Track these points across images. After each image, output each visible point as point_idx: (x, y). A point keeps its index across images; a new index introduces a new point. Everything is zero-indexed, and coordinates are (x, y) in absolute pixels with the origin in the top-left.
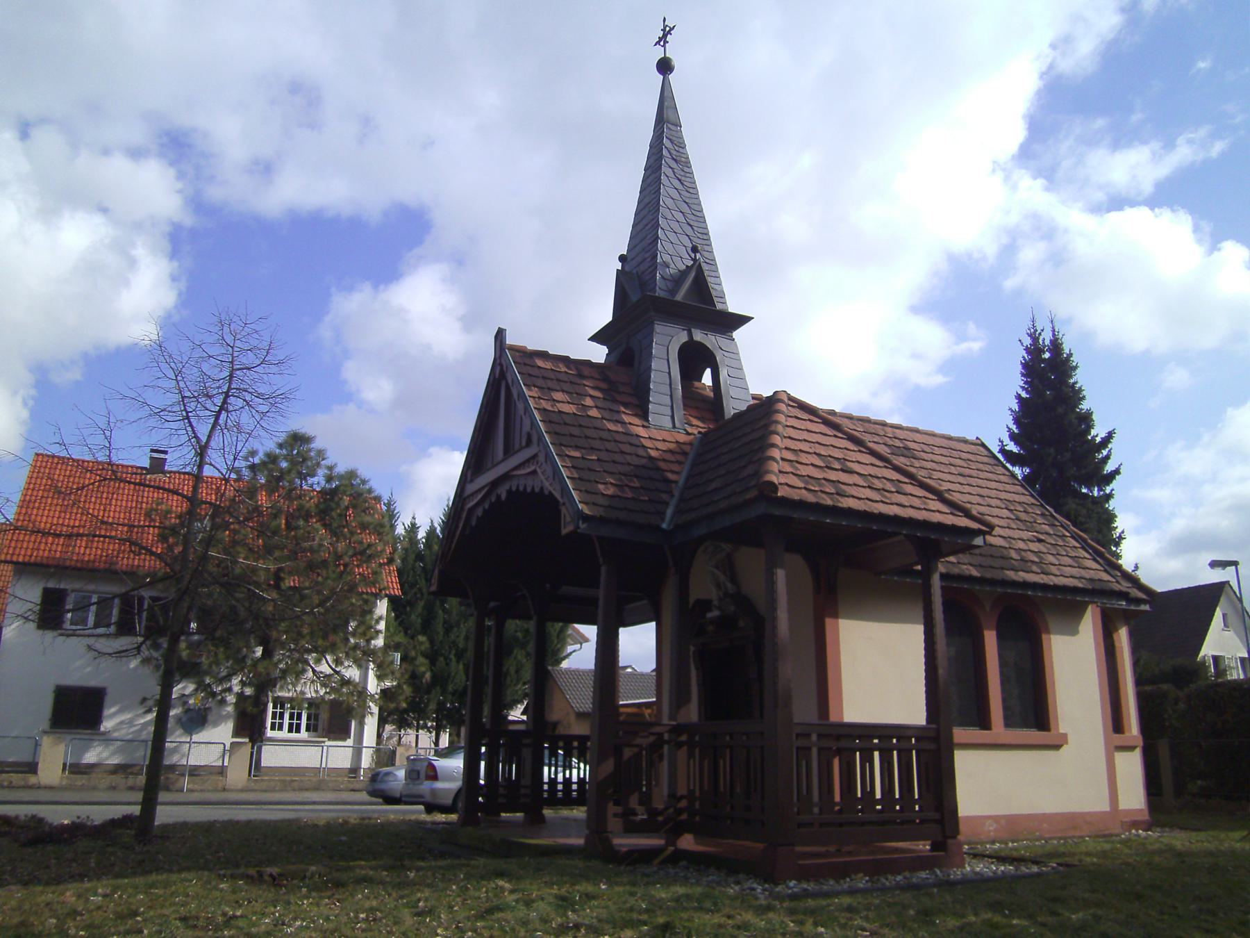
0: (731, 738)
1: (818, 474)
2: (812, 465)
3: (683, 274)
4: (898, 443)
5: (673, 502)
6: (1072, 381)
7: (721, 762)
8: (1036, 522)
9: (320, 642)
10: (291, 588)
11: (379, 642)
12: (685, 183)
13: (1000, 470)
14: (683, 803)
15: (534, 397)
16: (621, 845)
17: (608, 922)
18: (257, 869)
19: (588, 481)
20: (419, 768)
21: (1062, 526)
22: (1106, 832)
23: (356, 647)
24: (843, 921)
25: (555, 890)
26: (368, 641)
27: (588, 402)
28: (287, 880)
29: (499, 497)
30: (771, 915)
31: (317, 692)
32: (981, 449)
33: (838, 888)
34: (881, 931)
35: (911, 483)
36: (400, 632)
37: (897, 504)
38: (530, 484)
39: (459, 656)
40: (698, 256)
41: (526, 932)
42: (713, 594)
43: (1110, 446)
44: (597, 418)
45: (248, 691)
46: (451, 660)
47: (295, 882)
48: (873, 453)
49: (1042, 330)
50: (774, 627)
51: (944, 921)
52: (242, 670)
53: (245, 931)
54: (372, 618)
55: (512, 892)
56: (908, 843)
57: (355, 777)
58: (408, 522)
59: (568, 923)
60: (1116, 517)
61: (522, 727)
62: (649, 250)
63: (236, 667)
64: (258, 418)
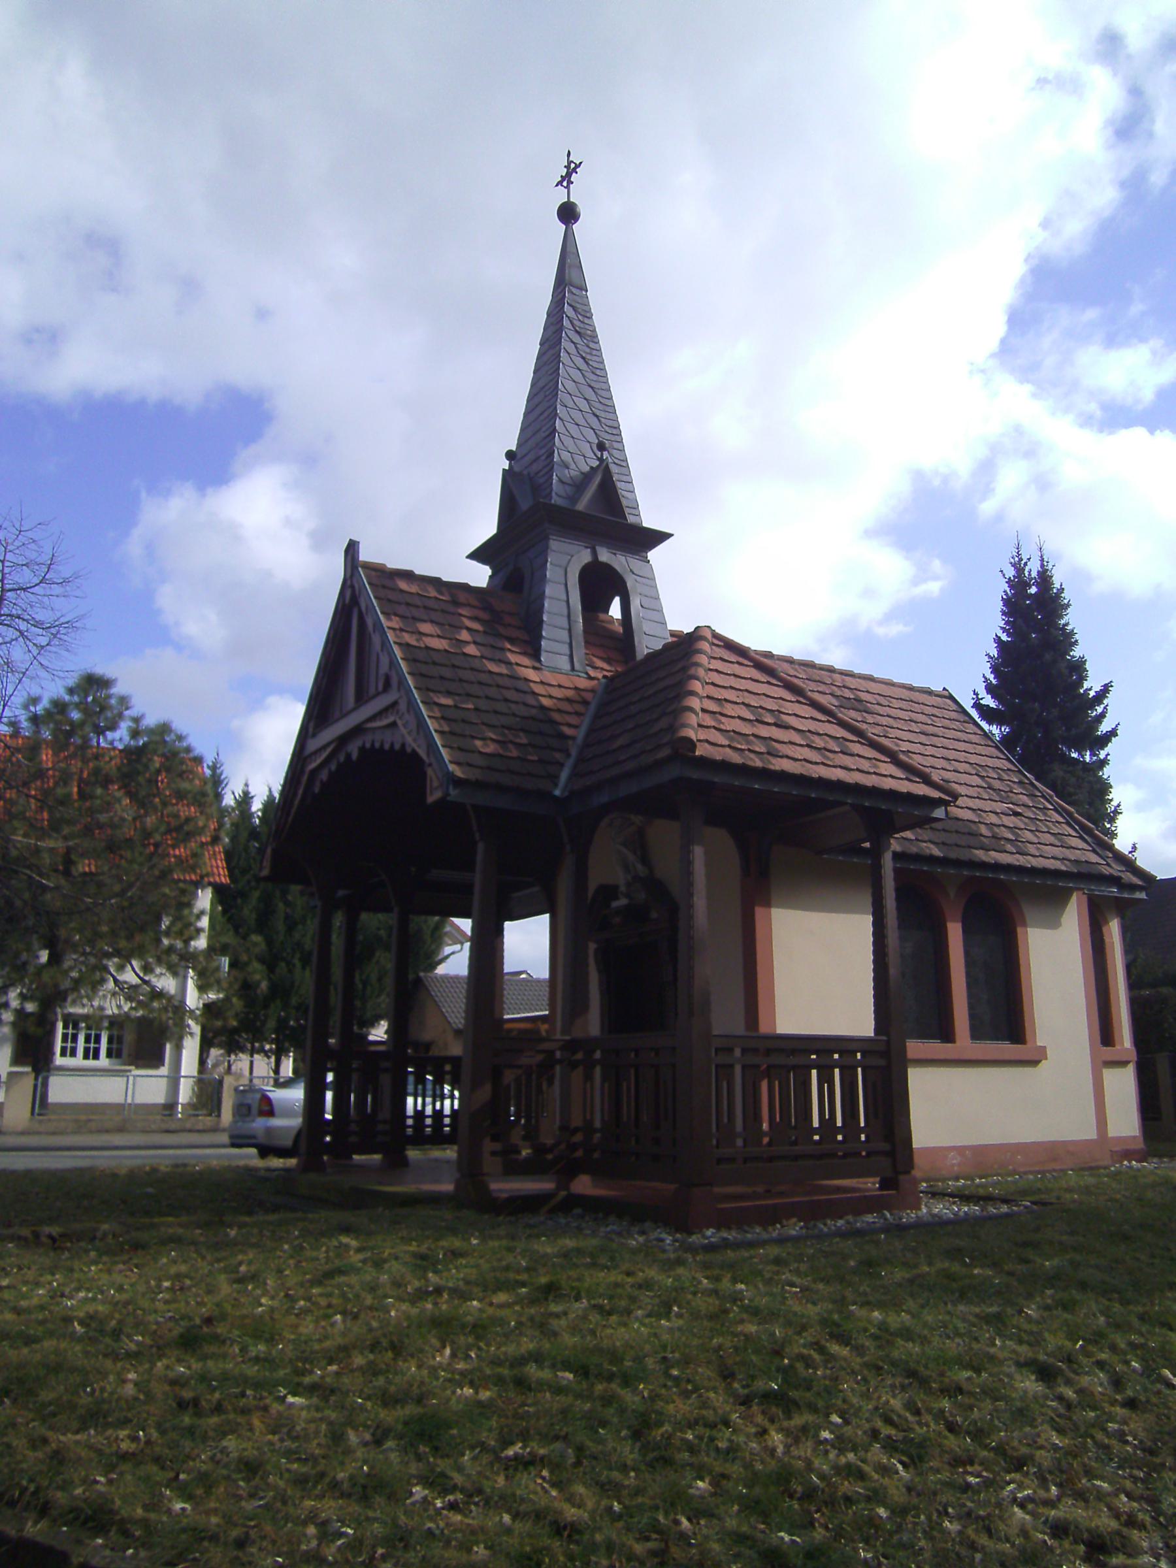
0: (636, 1055)
1: (746, 729)
2: (739, 717)
3: (587, 477)
4: (848, 694)
5: (569, 764)
6: (1062, 622)
7: (625, 1084)
8: (1012, 792)
9: (123, 944)
10: (85, 874)
11: (201, 943)
12: (591, 363)
13: (971, 728)
14: (578, 1138)
15: (394, 629)
16: (500, 1191)
17: (477, 1285)
18: (33, 1228)
19: (464, 736)
20: (249, 1101)
21: (1043, 797)
22: (1093, 1164)
23: (171, 949)
24: (767, 1275)
25: (413, 1247)
26: (187, 942)
27: (465, 635)
28: (72, 1242)
29: (348, 756)
30: (680, 1270)
31: (119, 1007)
32: (948, 701)
33: (765, 1236)
34: (813, 1286)
35: (859, 742)
36: (228, 930)
37: (841, 767)
38: (387, 740)
39: (305, 961)
40: (605, 454)
41: (374, 1298)
42: (620, 878)
43: (1105, 702)
44: (475, 657)
45: (30, 1007)
46: (294, 965)
47: (83, 1244)
48: (815, 705)
49: (1029, 559)
50: (690, 917)
51: (892, 1273)
52: (21, 980)
53: (12, 1304)
54: (191, 912)
55: (359, 1250)
56: (855, 1180)
57: (170, 1115)
58: (239, 792)
59: (428, 1286)
60: (1111, 787)
61: (382, 1048)
62: (544, 447)
63: (13, 975)
64: (35, 651)
